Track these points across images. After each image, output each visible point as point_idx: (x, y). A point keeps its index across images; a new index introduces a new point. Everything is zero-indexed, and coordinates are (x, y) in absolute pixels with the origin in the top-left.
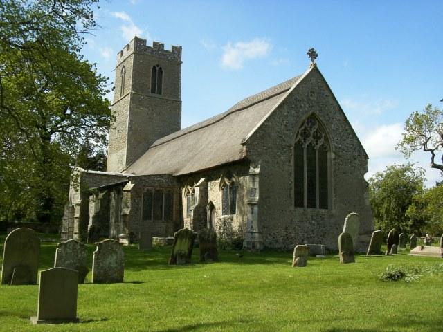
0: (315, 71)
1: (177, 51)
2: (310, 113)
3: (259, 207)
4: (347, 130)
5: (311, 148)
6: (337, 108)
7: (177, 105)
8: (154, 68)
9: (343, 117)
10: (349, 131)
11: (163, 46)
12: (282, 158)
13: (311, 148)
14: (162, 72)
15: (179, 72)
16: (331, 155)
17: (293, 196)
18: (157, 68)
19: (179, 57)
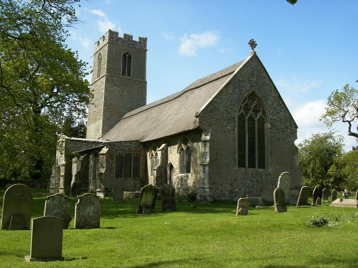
0: (255, 57)
1: (143, 41)
2: (250, 92)
4: (280, 105)
5: (251, 119)
6: (272, 87)
11: (132, 37)
12: (228, 127)
13: (251, 119)
15: (145, 58)
16: (268, 126)
17: (237, 158)
18: (127, 55)
19: (145, 46)
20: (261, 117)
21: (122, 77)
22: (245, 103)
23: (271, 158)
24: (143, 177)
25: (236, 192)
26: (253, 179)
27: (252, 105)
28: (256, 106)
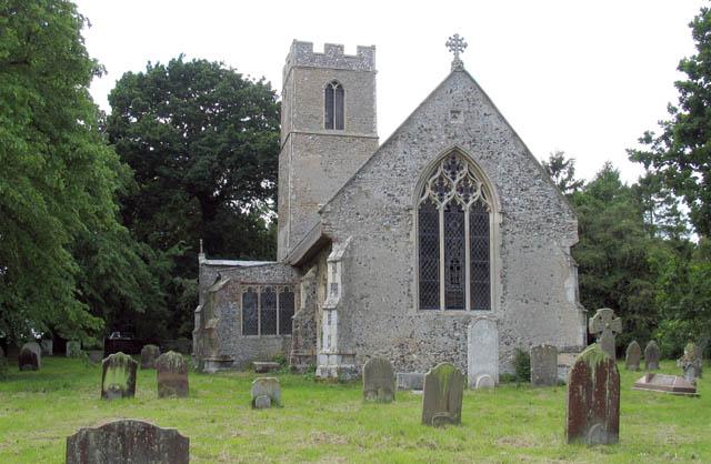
0: (458, 70)
1: (368, 53)
3: (339, 312)
4: (530, 171)
5: (454, 210)
6: (508, 135)
8: (329, 89)
11: (342, 47)
13: (454, 210)
14: (343, 91)
15: (372, 89)
16: (495, 219)
18: (335, 87)
19: (372, 63)
20: (478, 201)
21: (326, 132)
23: (505, 288)
25: (412, 362)
26: (457, 334)
27: (454, 179)
28: (466, 179)
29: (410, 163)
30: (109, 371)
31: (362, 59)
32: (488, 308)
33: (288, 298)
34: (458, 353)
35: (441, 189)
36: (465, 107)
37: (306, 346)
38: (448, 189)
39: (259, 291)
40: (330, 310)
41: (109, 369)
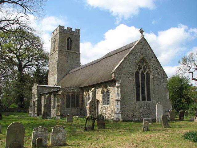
1: (78, 31)
2: (142, 57)
5: (142, 73)
6: (153, 55)
7: (78, 55)
8: (68, 39)
9: (156, 59)
10: (159, 65)
11: (72, 29)
13: (142, 73)
16: (151, 77)
17: (135, 96)
18: (69, 39)
19: (79, 33)
22: (139, 65)
24: (81, 107)
29: (133, 61)
30: (88, 121)
31: (77, 32)
32: (150, 101)
33: (78, 97)
34: (178, 115)
35: (140, 68)
36: (144, 47)
37: (93, 111)
38: (141, 68)
39: (70, 95)
40: (118, 101)
41: (88, 120)
